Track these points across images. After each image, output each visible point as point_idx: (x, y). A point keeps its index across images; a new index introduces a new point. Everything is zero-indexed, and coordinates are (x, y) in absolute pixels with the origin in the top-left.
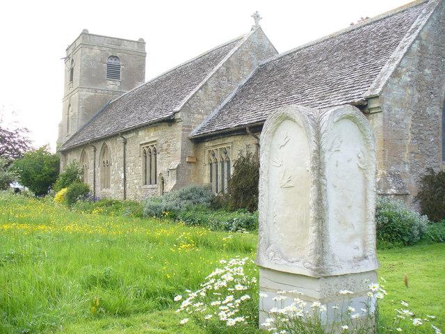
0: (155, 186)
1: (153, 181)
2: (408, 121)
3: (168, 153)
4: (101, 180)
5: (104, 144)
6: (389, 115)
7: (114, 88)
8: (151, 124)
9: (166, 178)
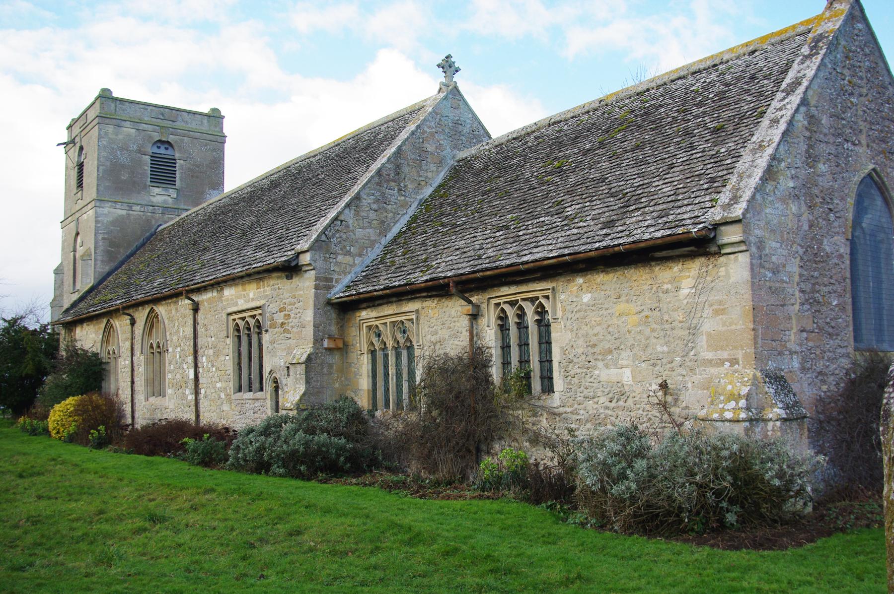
0: (259, 394)
1: (256, 385)
2: (794, 267)
3: (288, 332)
4: (147, 381)
5: (152, 310)
6: (760, 257)
7: (165, 202)
8: (249, 275)
9: (283, 381)
